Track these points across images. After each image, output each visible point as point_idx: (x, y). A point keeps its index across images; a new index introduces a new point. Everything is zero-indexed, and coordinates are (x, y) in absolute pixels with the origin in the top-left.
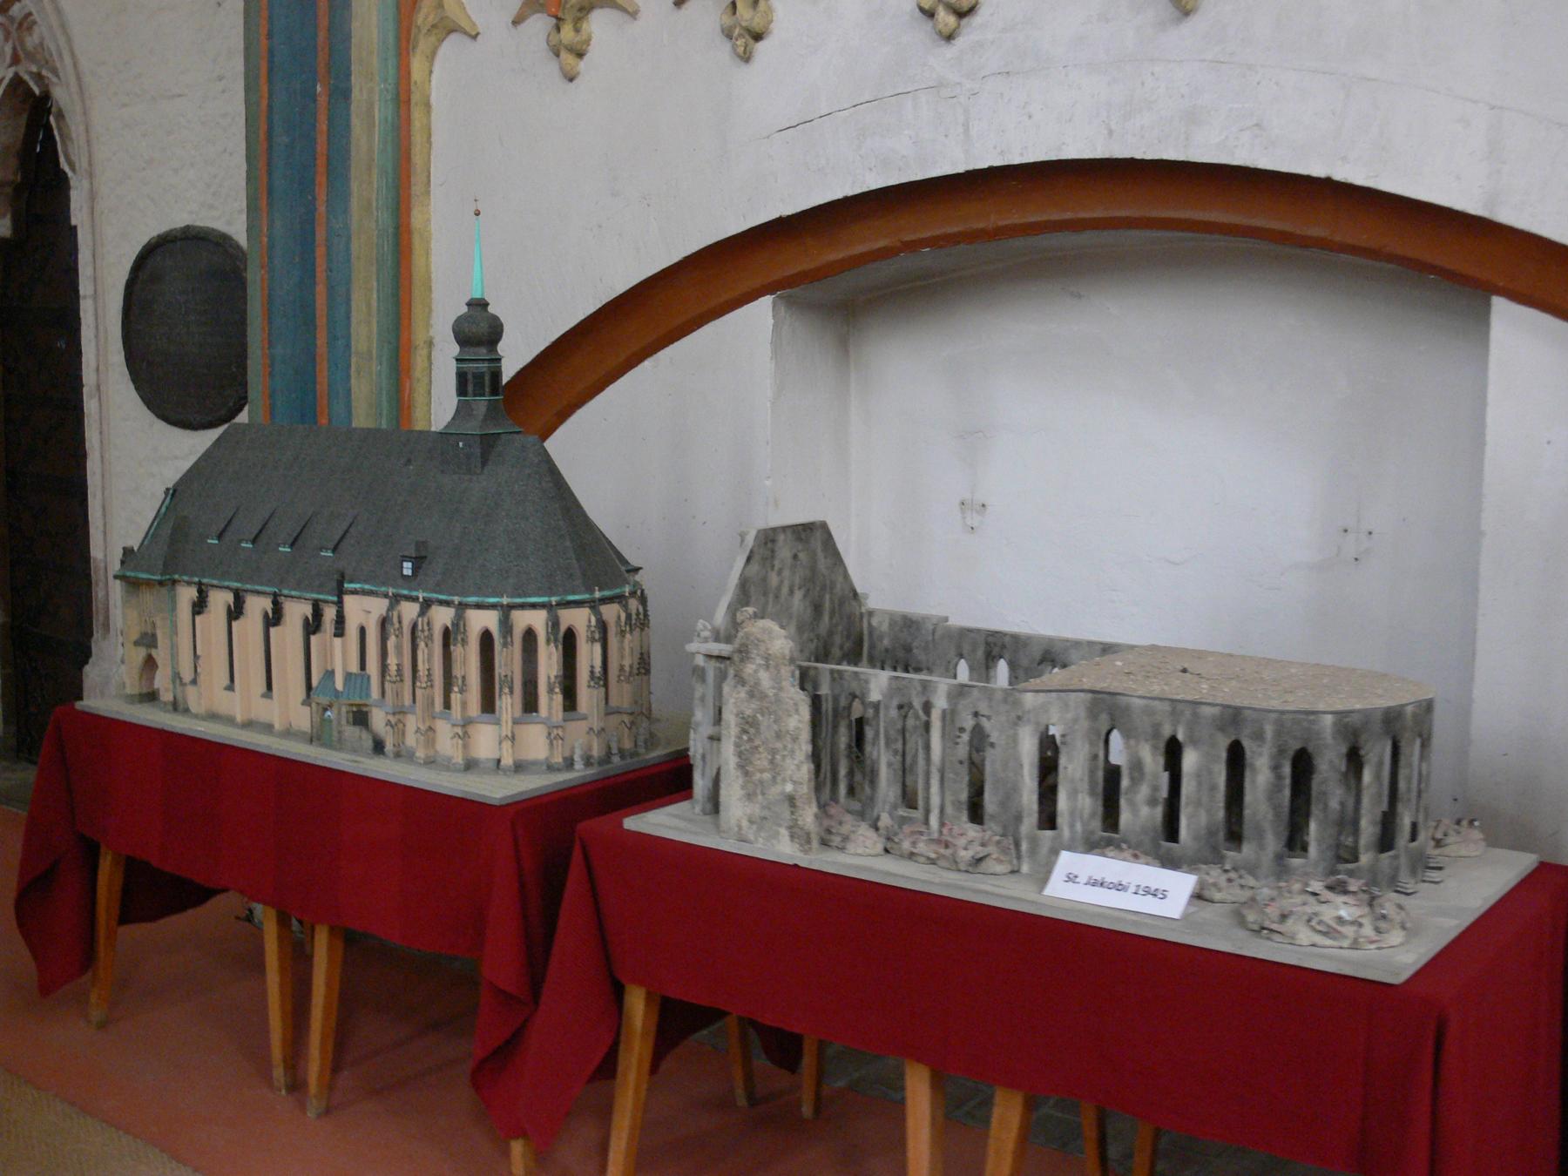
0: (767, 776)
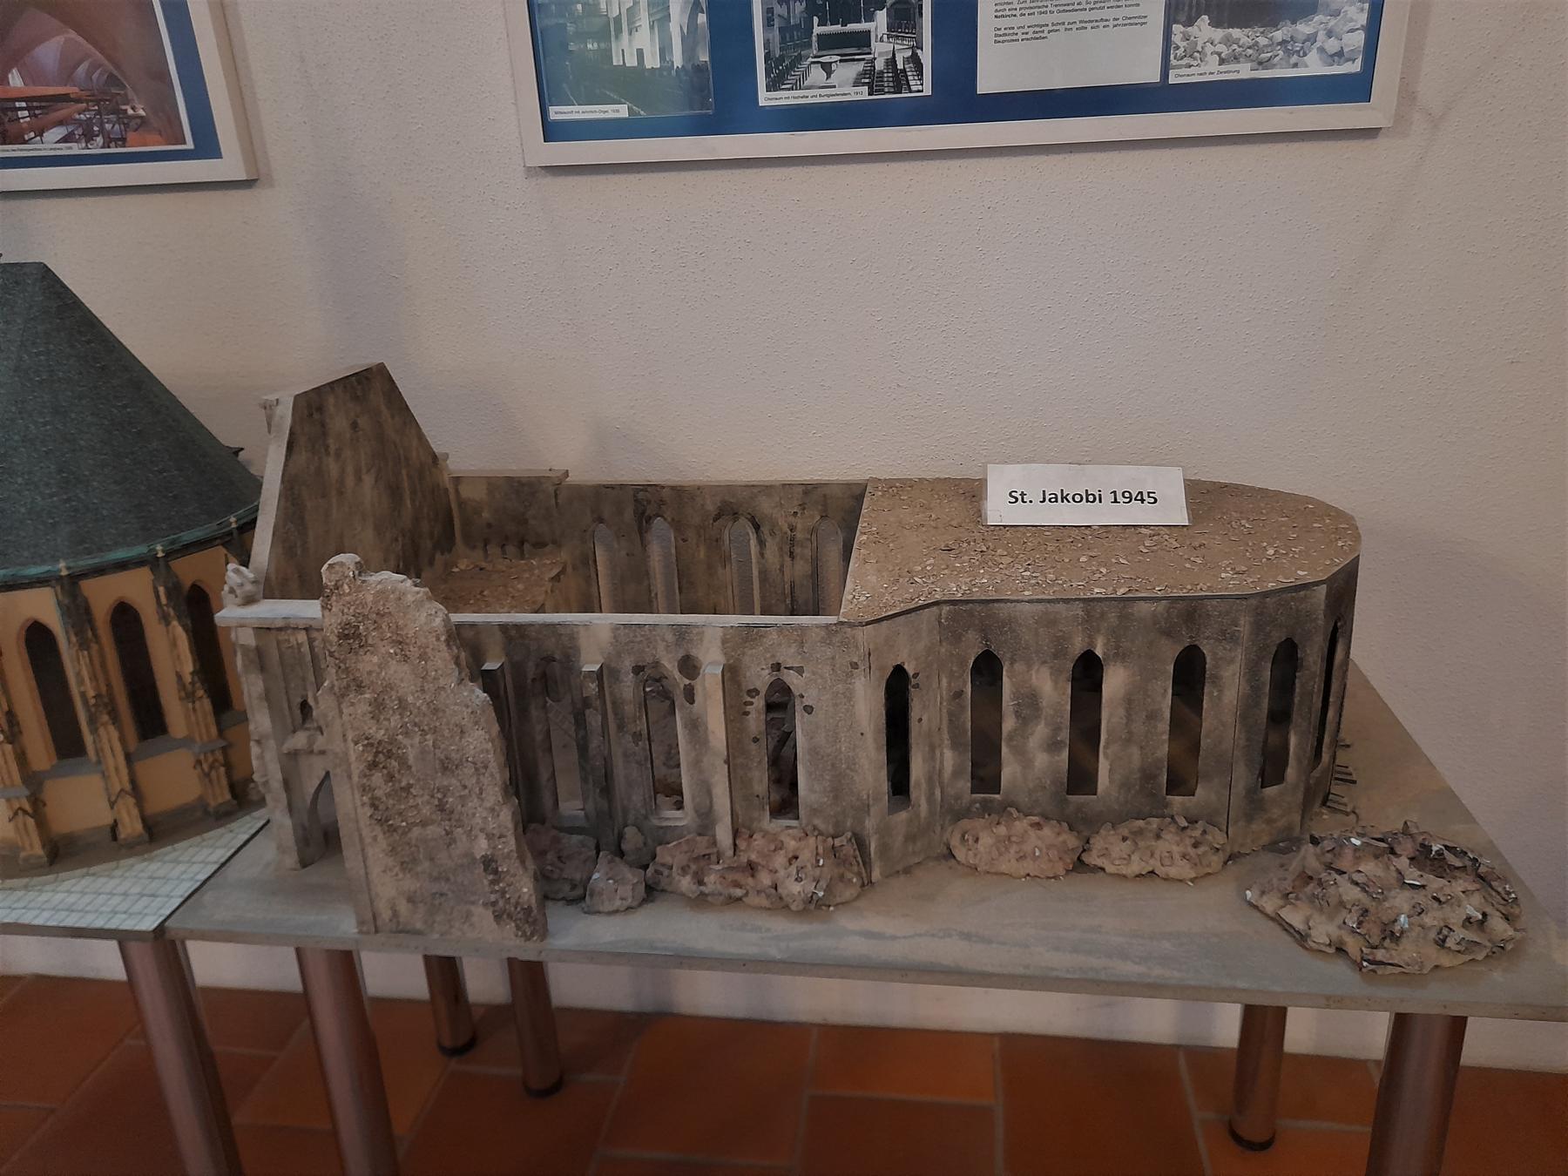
0: (434, 831)
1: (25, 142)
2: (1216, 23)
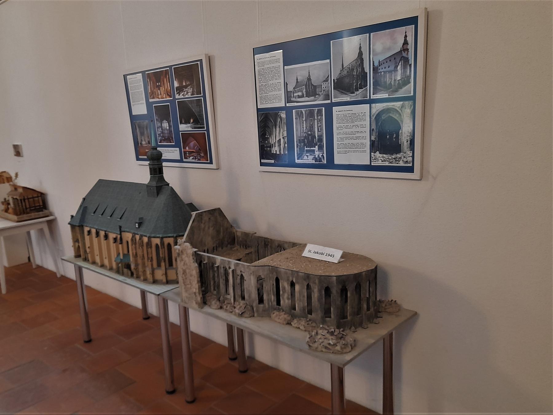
0: (189, 286)
2: (380, 153)
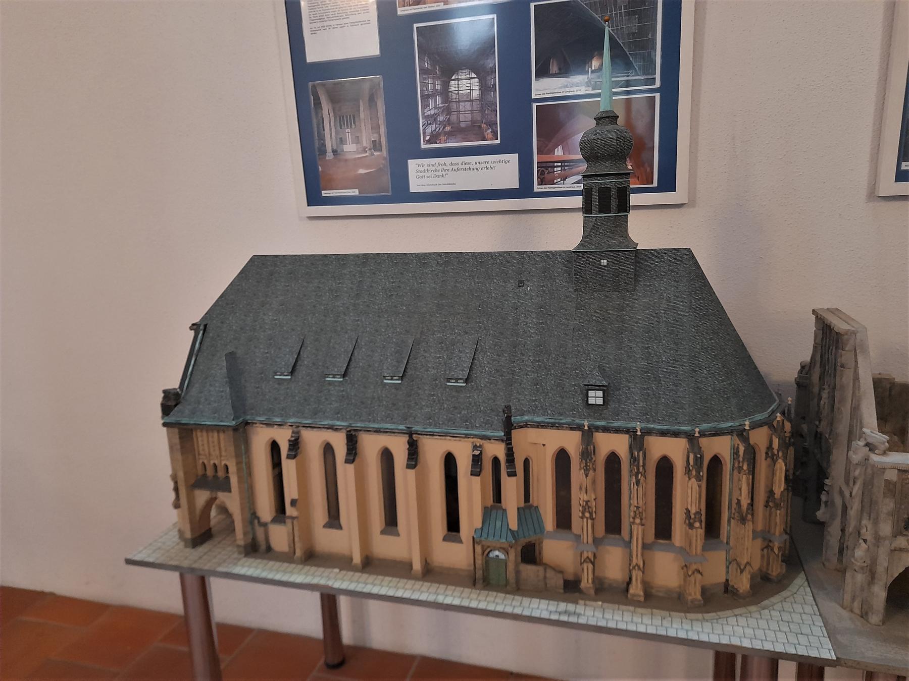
1: (554, 184)
